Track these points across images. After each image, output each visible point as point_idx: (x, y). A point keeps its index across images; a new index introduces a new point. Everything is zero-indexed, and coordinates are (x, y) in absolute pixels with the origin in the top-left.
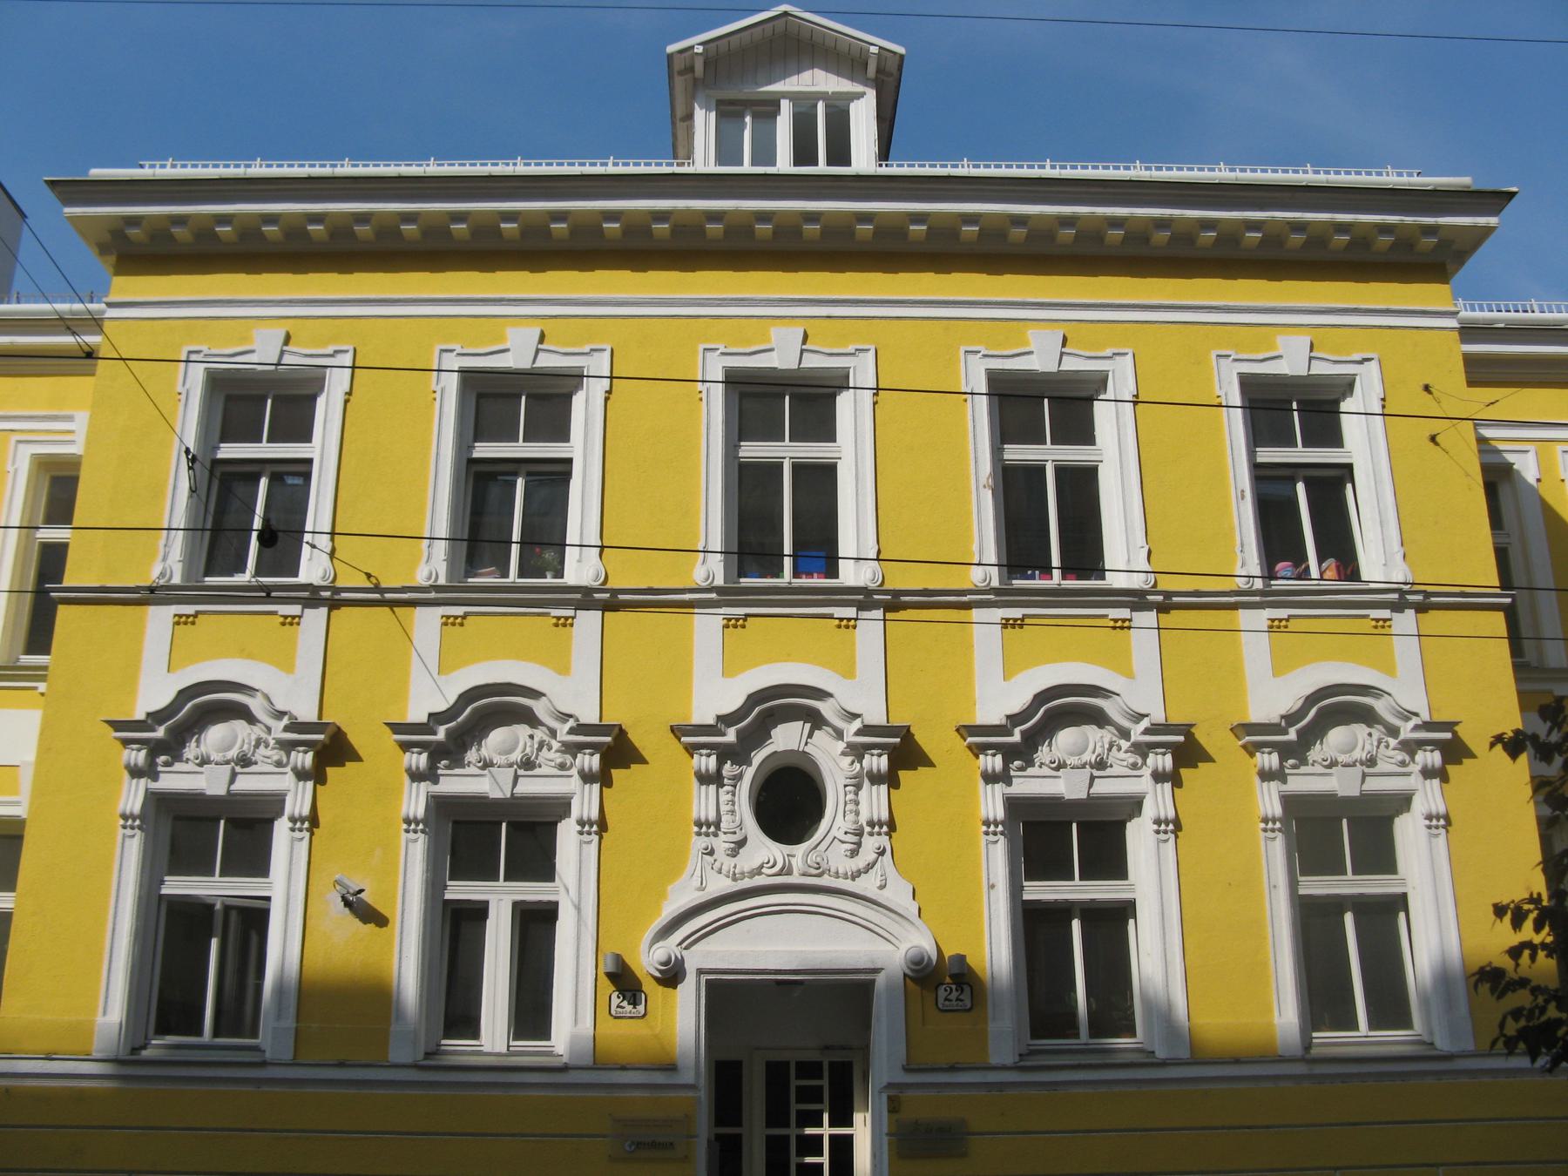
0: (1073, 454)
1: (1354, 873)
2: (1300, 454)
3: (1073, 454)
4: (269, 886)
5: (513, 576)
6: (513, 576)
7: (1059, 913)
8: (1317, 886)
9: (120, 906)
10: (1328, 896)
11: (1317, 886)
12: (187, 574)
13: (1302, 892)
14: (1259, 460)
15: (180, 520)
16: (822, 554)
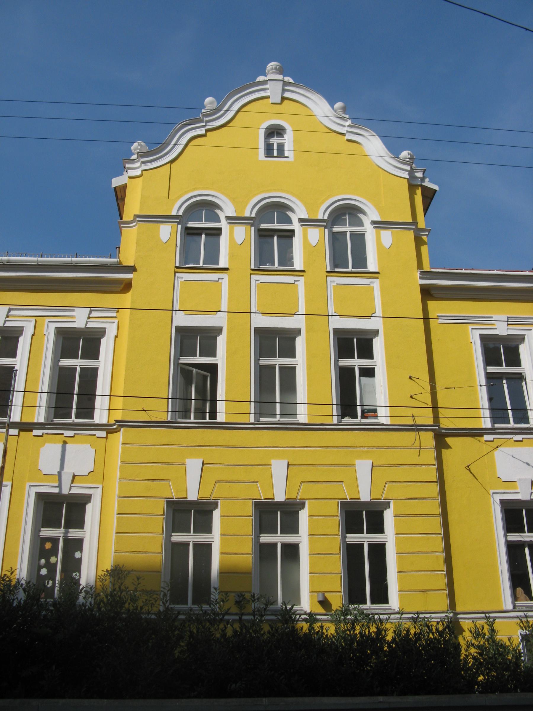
0: (287, 361)
1: (528, 532)
2: (504, 369)
3: (287, 361)
4: (115, 556)
5: (208, 420)
6: (192, 419)
7: (521, 545)
8: (514, 537)
9: (500, 544)
10: (518, 541)
11: (514, 537)
12: (47, 417)
13: (509, 539)
14: (488, 371)
15: (46, 389)
16: (365, 407)
